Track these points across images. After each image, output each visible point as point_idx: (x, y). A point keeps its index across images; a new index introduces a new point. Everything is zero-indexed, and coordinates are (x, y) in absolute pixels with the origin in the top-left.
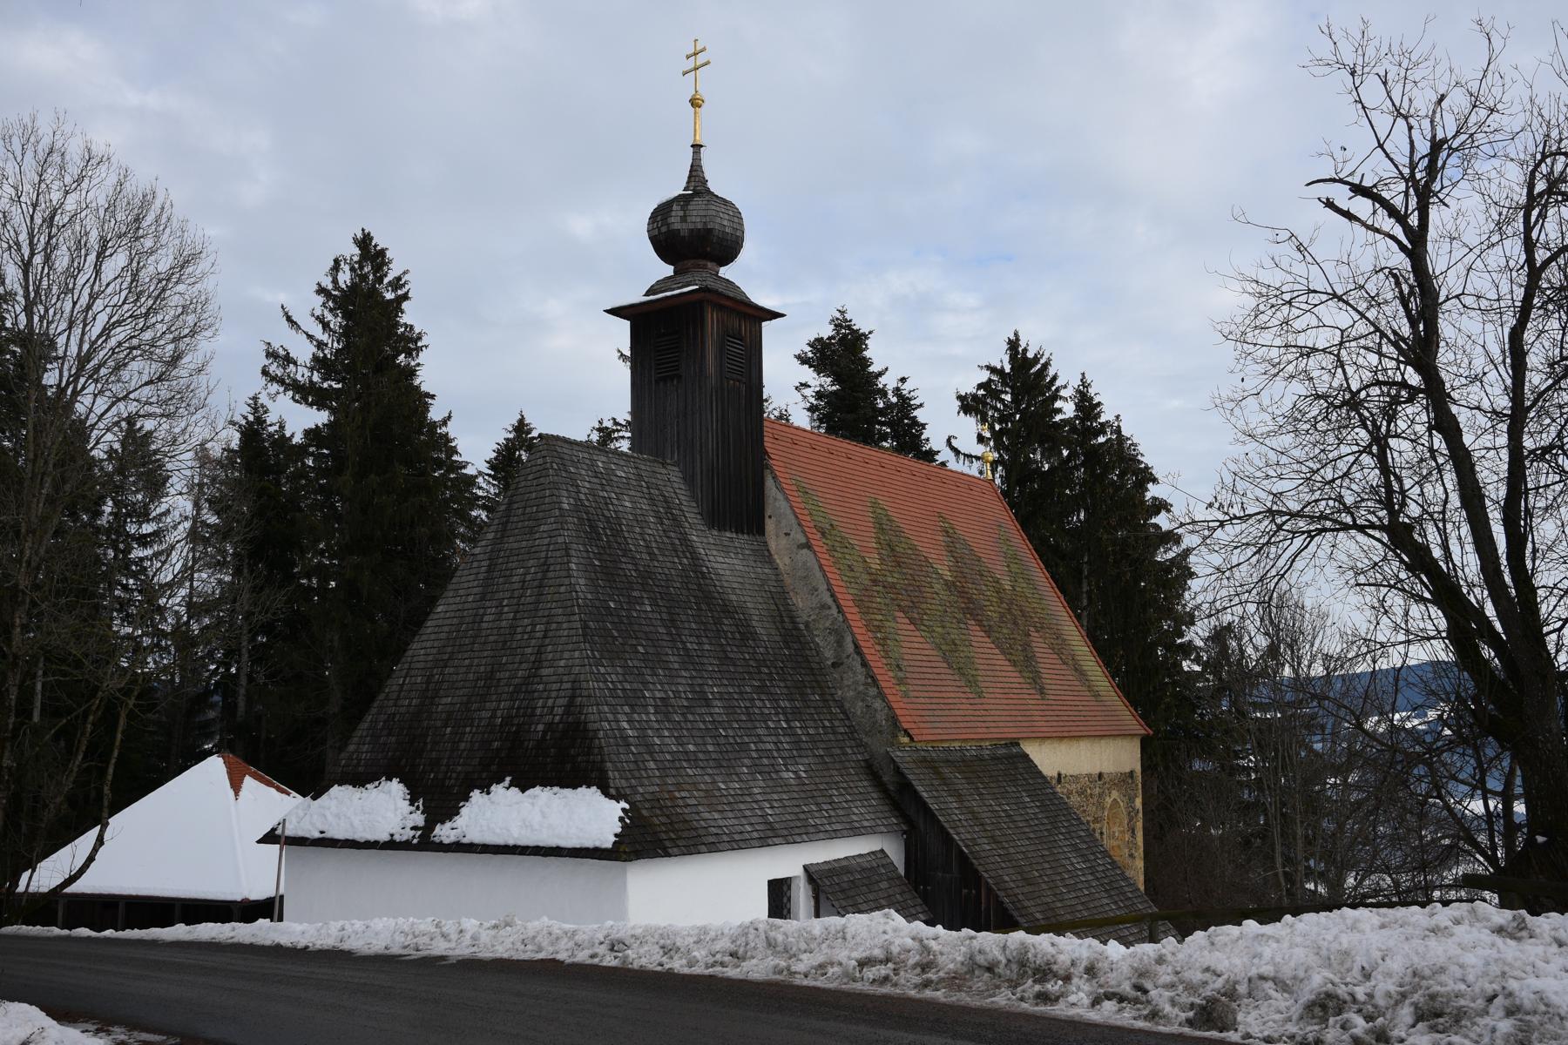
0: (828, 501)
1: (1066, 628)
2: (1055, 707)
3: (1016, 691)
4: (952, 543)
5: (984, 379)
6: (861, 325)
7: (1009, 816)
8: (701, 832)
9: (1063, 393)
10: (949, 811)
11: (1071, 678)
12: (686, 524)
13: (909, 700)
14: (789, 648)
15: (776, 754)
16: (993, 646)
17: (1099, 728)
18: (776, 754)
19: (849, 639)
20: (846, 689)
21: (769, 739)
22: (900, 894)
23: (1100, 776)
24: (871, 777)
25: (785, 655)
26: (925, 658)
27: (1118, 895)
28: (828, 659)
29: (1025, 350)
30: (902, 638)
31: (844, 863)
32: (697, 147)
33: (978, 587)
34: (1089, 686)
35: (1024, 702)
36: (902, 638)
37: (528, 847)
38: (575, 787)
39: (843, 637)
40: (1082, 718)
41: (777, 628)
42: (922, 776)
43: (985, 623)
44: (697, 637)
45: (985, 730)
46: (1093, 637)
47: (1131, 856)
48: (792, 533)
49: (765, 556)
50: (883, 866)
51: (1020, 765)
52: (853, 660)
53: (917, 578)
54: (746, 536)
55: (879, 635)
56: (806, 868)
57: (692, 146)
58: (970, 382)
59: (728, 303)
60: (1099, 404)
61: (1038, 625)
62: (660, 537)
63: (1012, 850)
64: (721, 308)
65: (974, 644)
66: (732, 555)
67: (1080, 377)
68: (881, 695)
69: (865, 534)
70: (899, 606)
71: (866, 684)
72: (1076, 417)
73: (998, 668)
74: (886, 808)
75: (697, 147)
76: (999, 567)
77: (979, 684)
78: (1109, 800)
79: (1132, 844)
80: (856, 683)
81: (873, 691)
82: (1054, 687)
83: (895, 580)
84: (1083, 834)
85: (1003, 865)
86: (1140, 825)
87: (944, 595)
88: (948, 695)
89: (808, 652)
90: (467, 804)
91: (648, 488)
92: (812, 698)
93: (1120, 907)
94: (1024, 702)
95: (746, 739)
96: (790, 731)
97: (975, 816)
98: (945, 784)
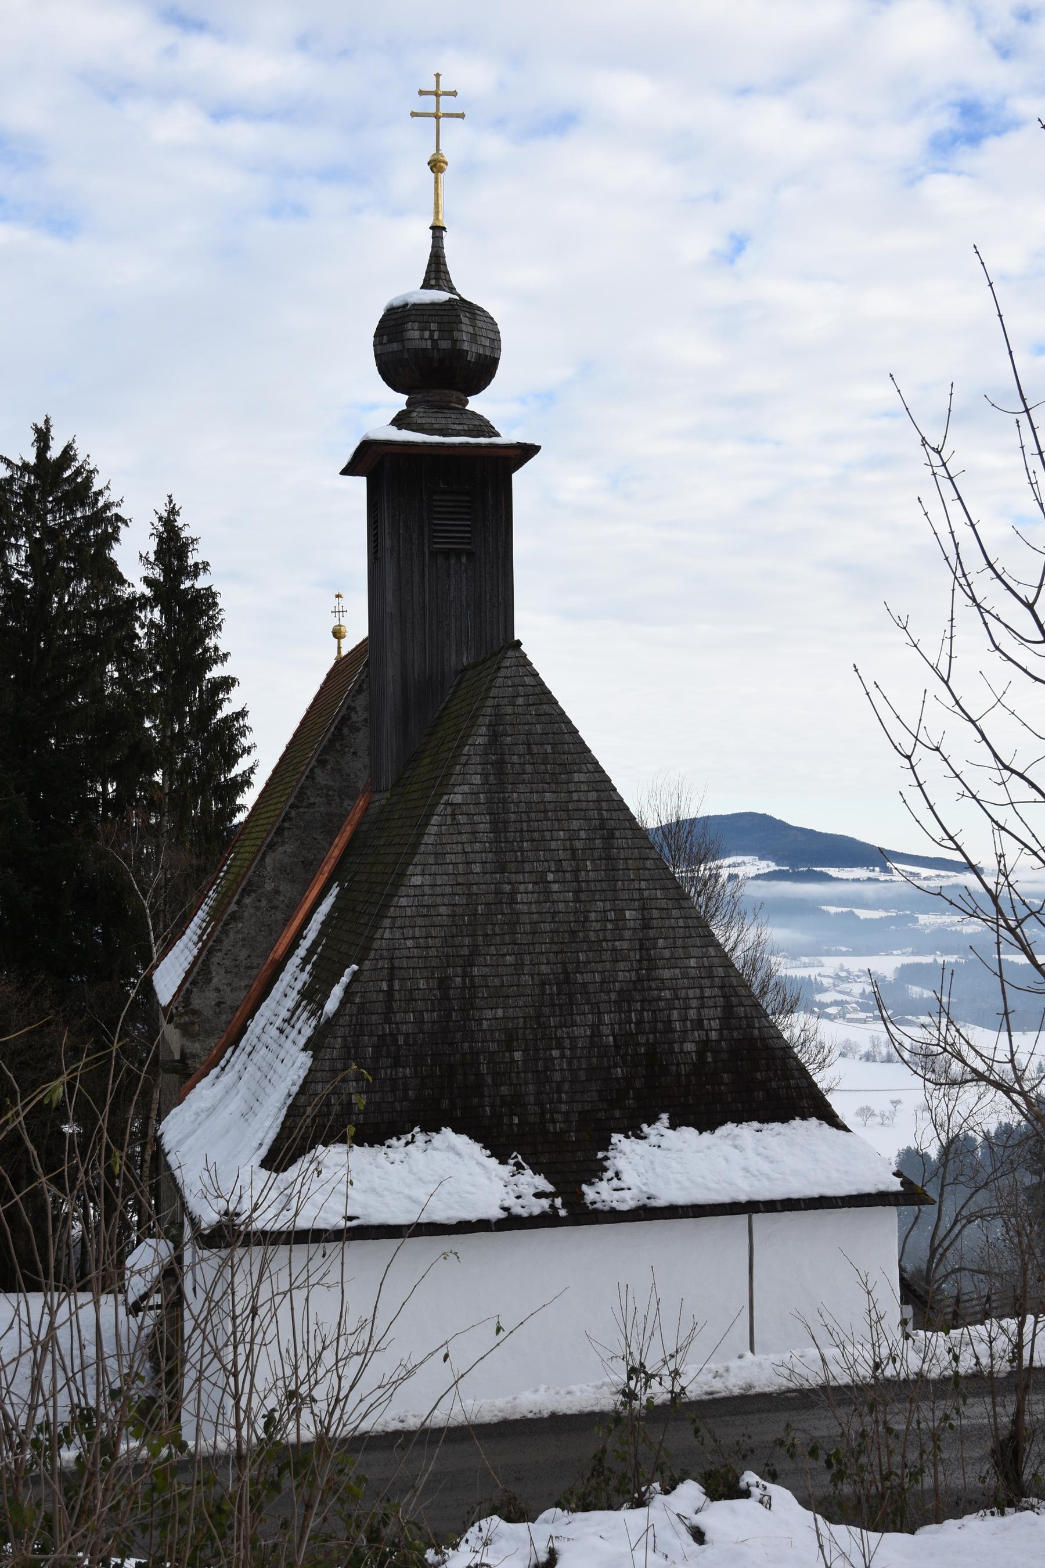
32: (438, 231)
38: (785, 1119)
67: (167, 500)
90: (610, 1154)
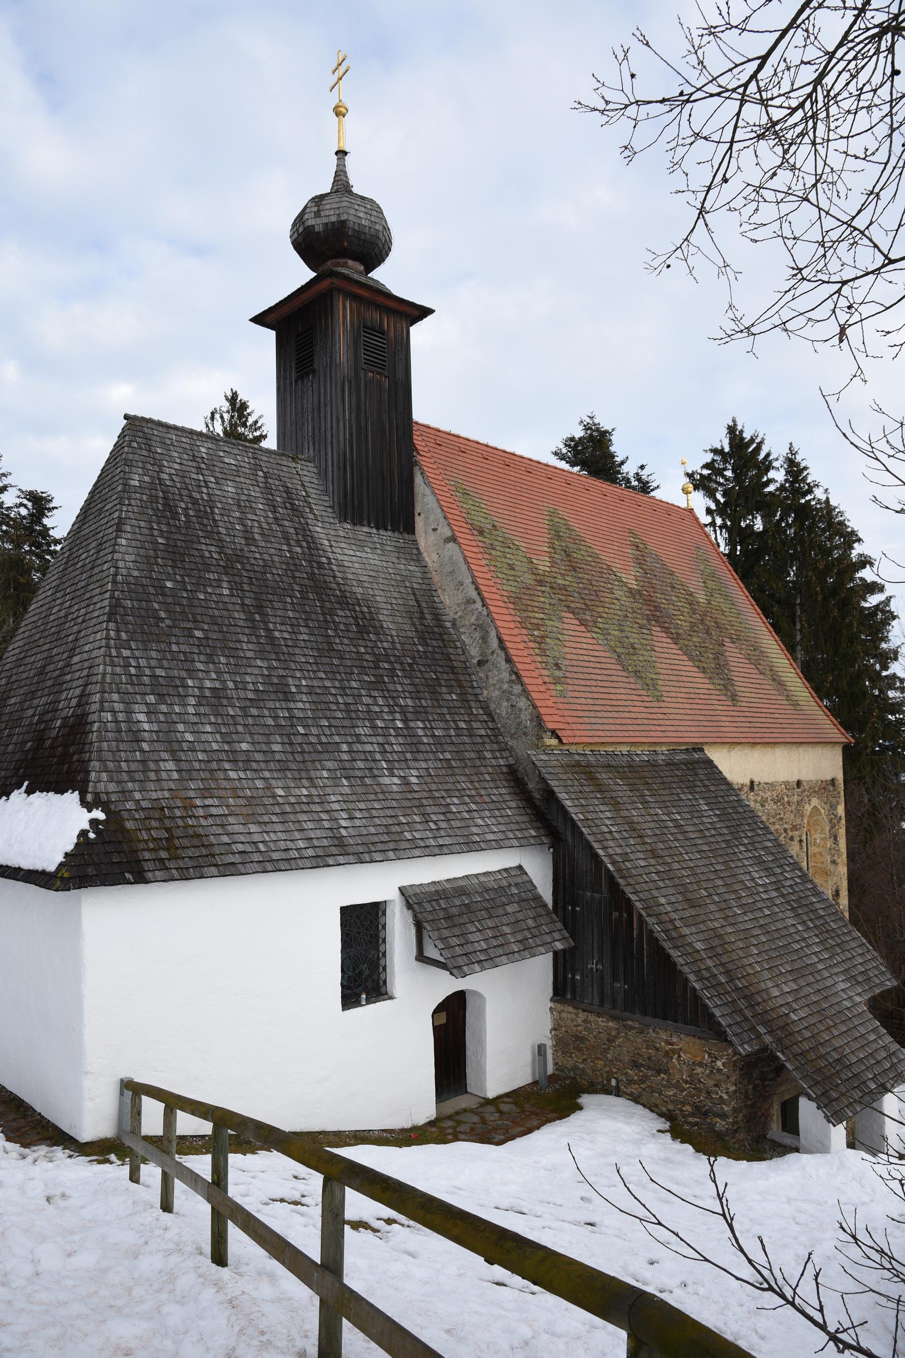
0: (494, 505)
1: (765, 641)
2: (747, 714)
3: (703, 697)
4: (641, 556)
5: (709, 460)
6: (606, 426)
7: (678, 826)
8: (216, 850)
9: (775, 464)
10: (598, 822)
11: (768, 687)
12: (311, 516)
13: (565, 700)
14: (425, 643)
15: (378, 756)
16: (680, 652)
17: (796, 735)
18: (378, 756)
19: (493, 634)
20: (492, 688)
21: (371, 739)
22: (534, 918)
23: (799, 783)
24: (512, 784)
25: (418, 651)
26: (592, 659)
27: (806, 913)
28: (473, 657)
29: (741, 432)
30: (567, 638)
31: (462, 883)
32: (341, 154)
33: (668, 597)
34: (787, 696)
35: (713, 707)
36: (567, 638)
37: (19, 869)
39: (487, 632)
40: (778, 725)
41: (414, 624)
42: (569, 782)
43: (673, 631)
44: (292, 625)
45: (660, 734)
46: (808, 672)
47: (834, 862)
48: (439, 528)
49: (416, 557)
50: (516, 885)
51: (700, 771)
52: (498, 655)
53: (594, 583)
54: (389, 533)
55: (536, 633)
56: (402, 890)
57: (337, 153)
58: (697, 462)
59: (364, 293)
60: (805, 468)
61: (734, 637)
62: (268, 524)
63: (676, 866)
64: (355, 298)
65: (656, 649)
66: (368, 550)
68: (525, 693)
69: (537, 538)
70: (568, 607)
71: (511, 681)
72: (786, 480)
73: (684, 673)
74: (525, 818)
75: (341, 154)
76: (693, 582)
77: (659, 688)
78: (808, 808)
79: (834, 851)
80: (501, 681)
81: (517, 689)
82: (747, 695)
83: (567, 583)
84: (769, 844)
85: (661, 884)
86: (842, 832)
87: (626, 601)
88: (618, 697)
89: (451, 650)
91: (266, 477)
92: (447, 697)
93: (809, 928)
94: (713, 707)
95: (337, 739)
96: (408, 732)
97: (632, 826)
98: (600, 791)
